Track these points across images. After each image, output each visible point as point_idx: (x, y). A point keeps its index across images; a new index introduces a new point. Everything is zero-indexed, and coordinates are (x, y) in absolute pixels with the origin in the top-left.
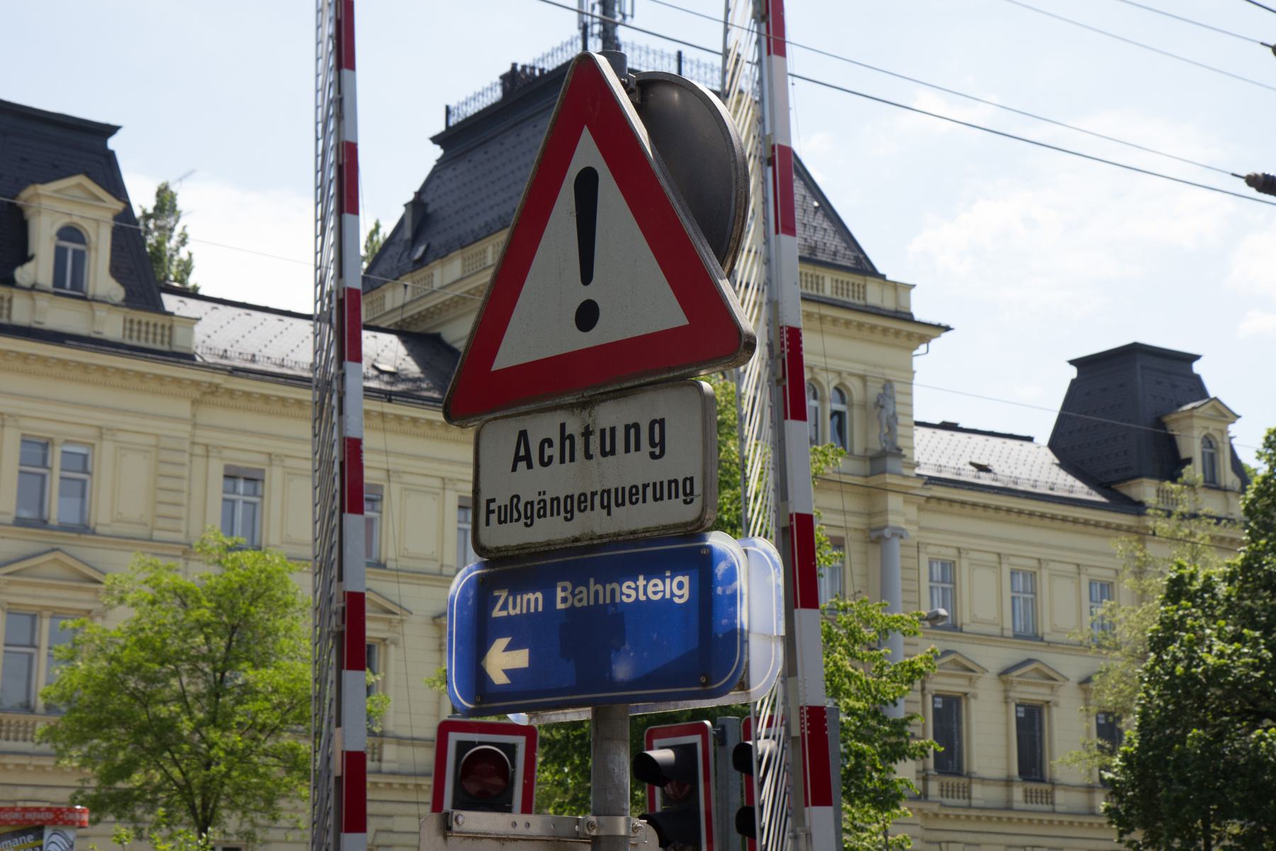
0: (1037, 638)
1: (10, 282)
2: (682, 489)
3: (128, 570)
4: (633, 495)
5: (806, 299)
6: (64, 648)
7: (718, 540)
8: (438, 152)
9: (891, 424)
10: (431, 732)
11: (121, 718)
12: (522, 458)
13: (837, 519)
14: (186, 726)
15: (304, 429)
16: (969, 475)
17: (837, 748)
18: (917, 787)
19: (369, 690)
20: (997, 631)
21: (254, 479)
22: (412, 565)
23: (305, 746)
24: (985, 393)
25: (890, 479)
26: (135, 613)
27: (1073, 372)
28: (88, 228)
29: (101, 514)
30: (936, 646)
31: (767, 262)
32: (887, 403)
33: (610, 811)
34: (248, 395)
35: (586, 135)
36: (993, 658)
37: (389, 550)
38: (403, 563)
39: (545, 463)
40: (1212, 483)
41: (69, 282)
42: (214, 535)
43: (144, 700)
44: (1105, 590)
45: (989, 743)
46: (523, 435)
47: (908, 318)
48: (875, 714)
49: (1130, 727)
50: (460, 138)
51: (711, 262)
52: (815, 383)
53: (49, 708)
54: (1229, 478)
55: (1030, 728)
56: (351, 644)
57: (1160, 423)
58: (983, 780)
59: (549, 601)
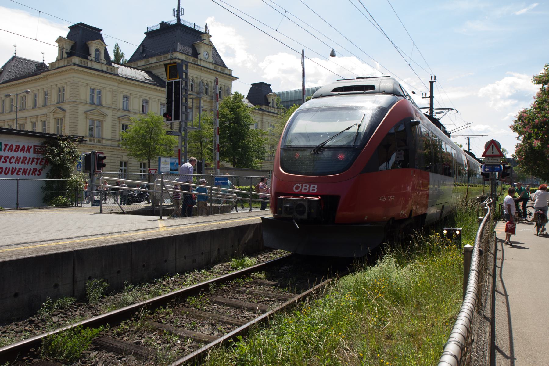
0: (129, 111)
1: (87, 59)
8: (145, 36)
20: (138, 112)
21: (128, 98)
28: (100, 49)
29: (103, 103)
38: (106, 106)
41: (97, 60)
47: (231, 76)
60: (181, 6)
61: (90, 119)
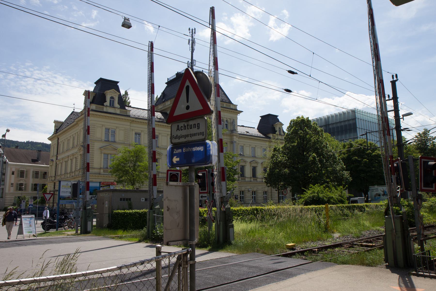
0: (255, 157)
1: (103, 105)
2: (202, 134)
3: (121, 148)
4: (195, 135)
5: (221, 107)
6: (112, 159)
7: (208, 141)
8: (166, 85)
9: (234, 126)
10: (166, 172)
11: (121, 170)
12: (178, 129)
13: (226, 140)
14: (130, 171)
15: (146, 127)
16: (246, 133)
17: (226, 173)
18: (238, 178)
19: (157, 165)
21: (139, 134)
22: (163, 147)
23: (147, 174)
24: (248, 121)
25: (234, 134)
26: (122, 154)
27: (260, 118)
28: (114, 97)
29: (117, 140)
30: (240, 159)
31: (216, 101)
32: (234, 122)
33: (192, 181)
34: (138, 122)
35: (187, 81)
36: (249, 160)
37: (159, 145)
39: (182, 130)
40: (280, 134)
41: (112, 105)
42: (134, 143)
43: (124, 167)
44: (265, 150)
45: (248, 172)
46: (178, 126)
47: (237, 110)
48: (232, 168)
49: (268, 170)
50: (170, 83)
51: (206, 99)
52: (223, 120)
53: (110, 168)
54: (282, 133)
55: (254, 170)
56: (154, 158)
57: (273, 125)
58: (247, 178)
59: (182, 151)
60: (194, 59)
61: (104, 154)
